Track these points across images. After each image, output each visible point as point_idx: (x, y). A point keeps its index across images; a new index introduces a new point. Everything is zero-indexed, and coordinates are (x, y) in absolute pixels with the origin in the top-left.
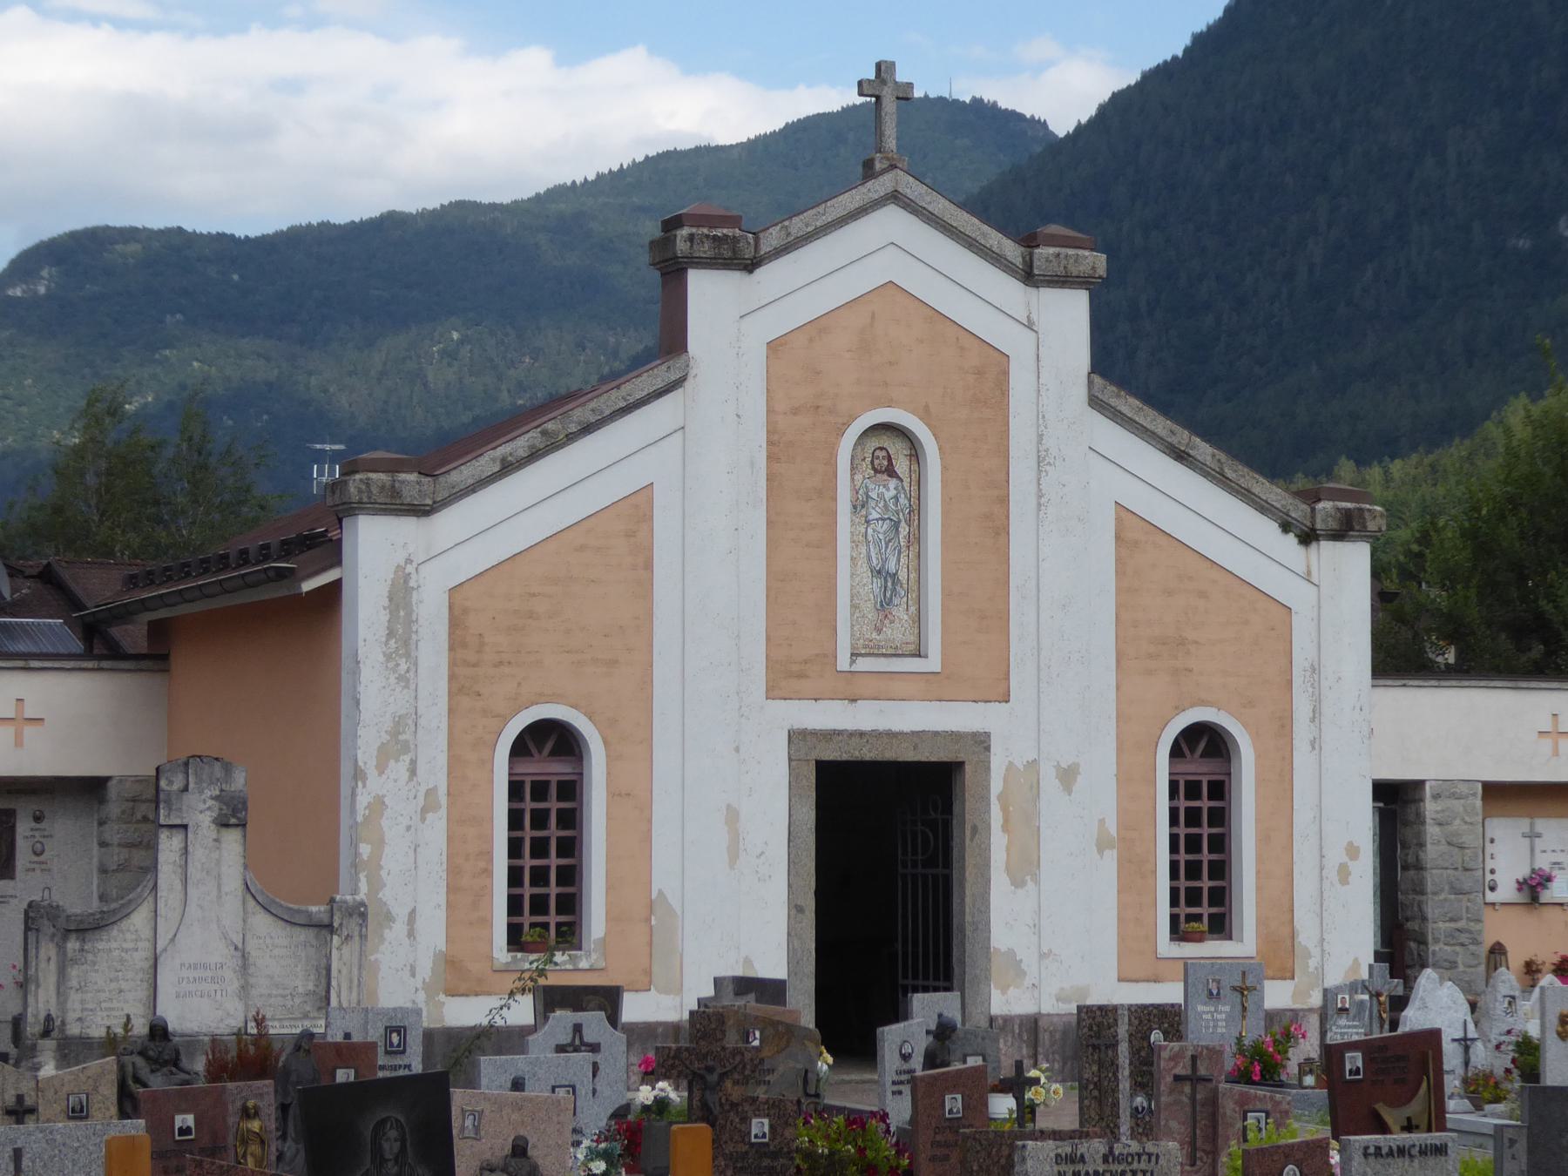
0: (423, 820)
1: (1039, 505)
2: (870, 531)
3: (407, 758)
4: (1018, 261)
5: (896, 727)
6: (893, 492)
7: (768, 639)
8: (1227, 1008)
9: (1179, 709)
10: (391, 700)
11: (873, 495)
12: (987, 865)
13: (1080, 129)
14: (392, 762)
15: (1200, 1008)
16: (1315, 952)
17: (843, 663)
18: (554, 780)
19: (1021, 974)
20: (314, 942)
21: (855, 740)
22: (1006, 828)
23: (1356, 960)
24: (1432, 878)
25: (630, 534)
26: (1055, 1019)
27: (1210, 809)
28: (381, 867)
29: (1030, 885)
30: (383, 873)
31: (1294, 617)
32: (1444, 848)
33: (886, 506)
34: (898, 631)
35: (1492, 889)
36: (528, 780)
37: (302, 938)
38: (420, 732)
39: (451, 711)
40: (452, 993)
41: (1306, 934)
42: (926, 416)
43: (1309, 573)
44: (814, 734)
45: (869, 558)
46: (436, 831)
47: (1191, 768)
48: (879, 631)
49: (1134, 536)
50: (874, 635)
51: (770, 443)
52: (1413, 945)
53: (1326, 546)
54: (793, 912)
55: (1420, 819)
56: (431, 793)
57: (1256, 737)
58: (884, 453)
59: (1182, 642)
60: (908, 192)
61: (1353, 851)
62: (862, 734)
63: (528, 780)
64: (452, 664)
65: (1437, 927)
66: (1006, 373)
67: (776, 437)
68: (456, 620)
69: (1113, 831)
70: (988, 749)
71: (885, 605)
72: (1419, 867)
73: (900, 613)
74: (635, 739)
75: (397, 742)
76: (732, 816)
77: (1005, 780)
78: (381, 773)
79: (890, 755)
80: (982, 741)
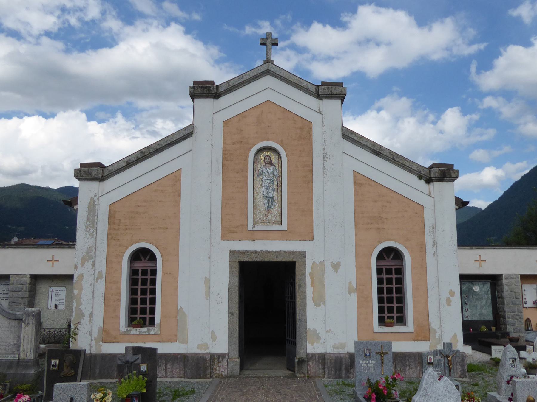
0: (97, 282)
1: (324, 172)
2: (263, 183)
3: (92, 261)
4: (314, 91)
5: (269, 250)
6: (272, 170)
7: (222, 220)
8: (374, 362)
9: (380, 242)
10: (87, 241)
11: (265, 171)
12: (305, 298)
13: (486, 209)
14: (86, 262)
15: (361, 362)
16: (438, 331)
17: (250, 227)
18: (149, 269)
19: (319, 338)
20: (17, 326)
21: (253, 255)
22: (312, 285)
23: (455, 334)
24: (506, 301)
25: (173, 186)
26: (332, 355)
27: (396, 278)
28: (81, 298)
29: (322, 305)
30: (82, 300)
31: (425, 209)
32: (509, 292)
33: (269, 175)
34: (274, 216)
35: (526, 303)
36: (140, 269)
37: (13, 324)
38: (97, 252)
39: (108, 245)
40: (105, 341)
41: (434, 324)
42: (281, 143)
43: (430, 193)
44: (238, 252)
45: (263, 192)
46: (101, 286)
47: (388, 264)
48: (267, 217)
49: (360, 182)
50: (265, 219)
51: (224, 154)
52: (502, 319)
53: (436, 184)
54: (230, 315)
55: (502, 285)
56: (100, 273)
57: (411, 252)
58: (268, 157)
59: (381, 218)
60: (273, 70)
61: (452, 293)
62: (256, 252)
63: (140, 269)
64: (109, 230)
65: (509, 314)
66: (311, 128)
67: (226, 152)
68: (111, 215)
69: (355, 286)
70: (305, 257)
71: (269, 208)
72: (502, 297)
73: (274, 211)
74: (173, 254)
75: (88, 255)
76: (207, 281)
77: (312, 268)
78: (82, 266)
79: (267, 259)
80: (303, 254)
